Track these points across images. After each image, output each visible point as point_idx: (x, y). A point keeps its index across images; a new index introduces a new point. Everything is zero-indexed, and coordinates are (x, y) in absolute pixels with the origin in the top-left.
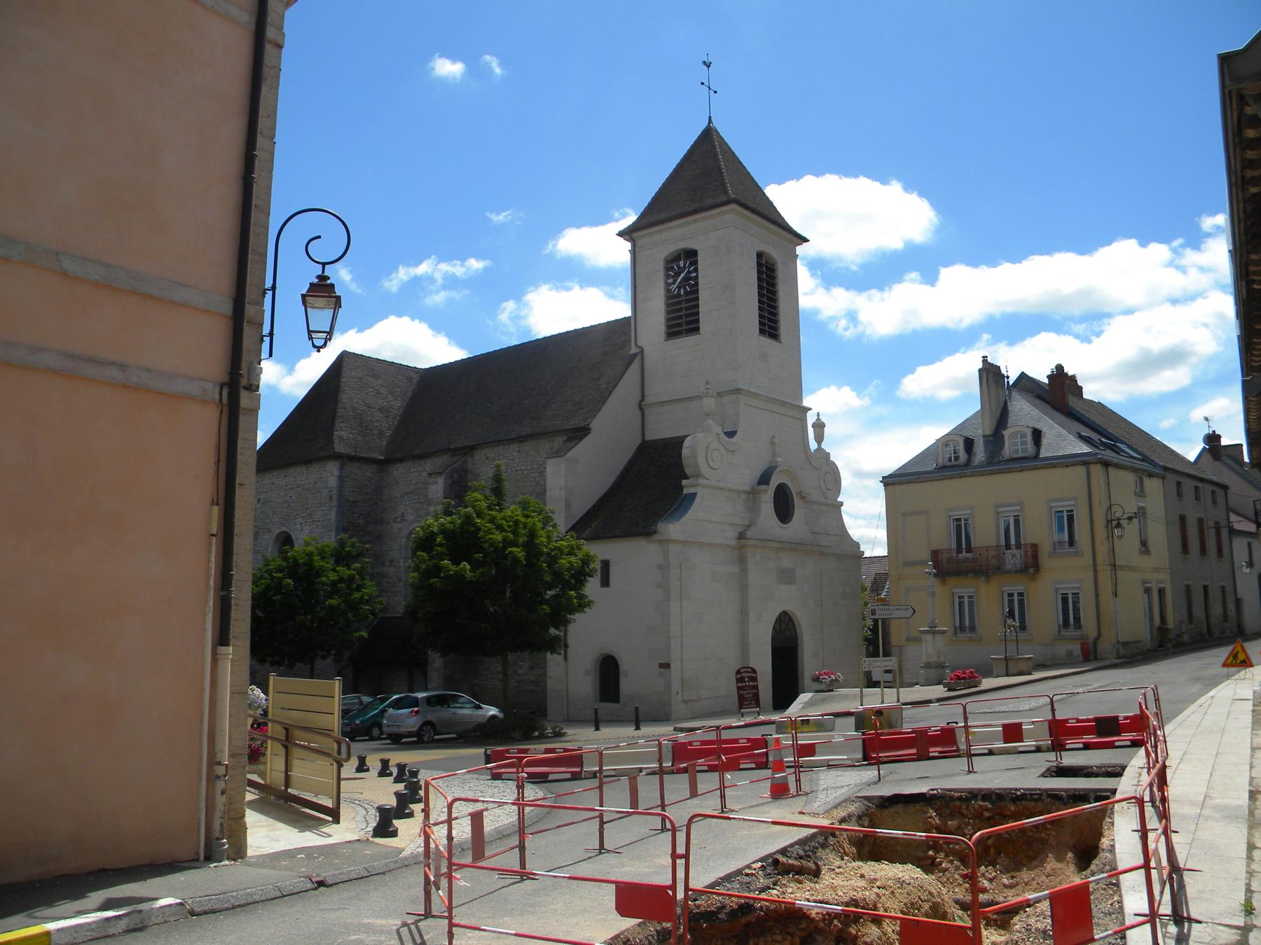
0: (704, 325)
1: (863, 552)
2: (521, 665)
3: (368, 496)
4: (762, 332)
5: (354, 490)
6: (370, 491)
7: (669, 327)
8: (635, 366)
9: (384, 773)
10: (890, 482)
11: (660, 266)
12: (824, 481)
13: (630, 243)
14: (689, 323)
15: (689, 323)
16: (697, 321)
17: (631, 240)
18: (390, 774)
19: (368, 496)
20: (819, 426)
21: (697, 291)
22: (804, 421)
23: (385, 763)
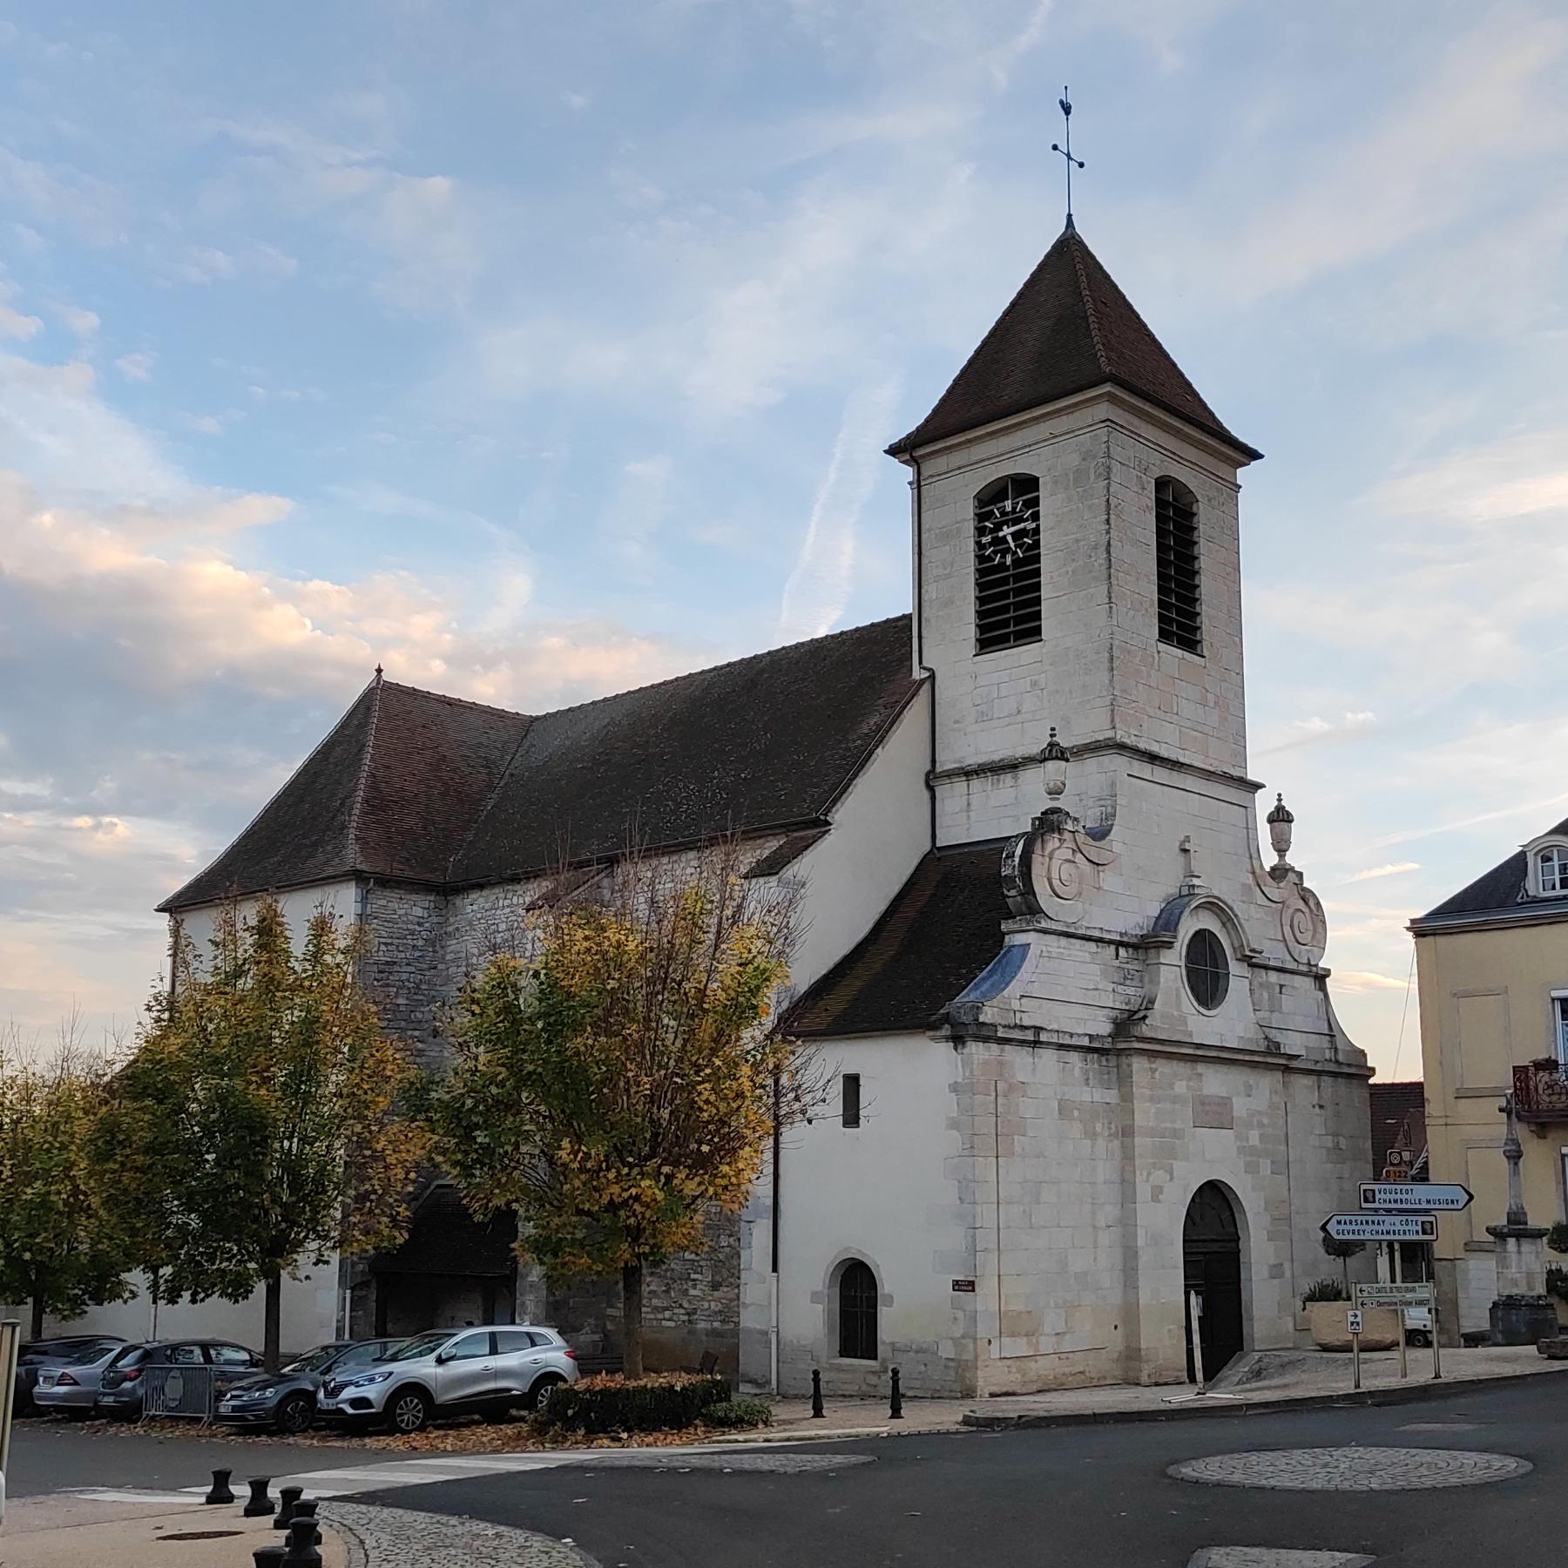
0: (1049, 622)
1: (1373, 1070)
2: (694, 1280)
3: (417, 954)
4: (1164, 636)
5: (389, 941)
6: (421, 943)
7: (982, 628)
8: (919, 705)
9: (258, 1506)
10: (1421, 929)
11: (969, 510)
12: (1292, 926)
13: (911, 469)
14: (1019, 620)
15: (1019, 620)
16: (1037, 616)
17: (915, 462)
18: (270, 1511)
19: (417, 954)
20: (1280, 817)
21: (1037, 558)
22: (1248, 809)
23: (259, 1487)
